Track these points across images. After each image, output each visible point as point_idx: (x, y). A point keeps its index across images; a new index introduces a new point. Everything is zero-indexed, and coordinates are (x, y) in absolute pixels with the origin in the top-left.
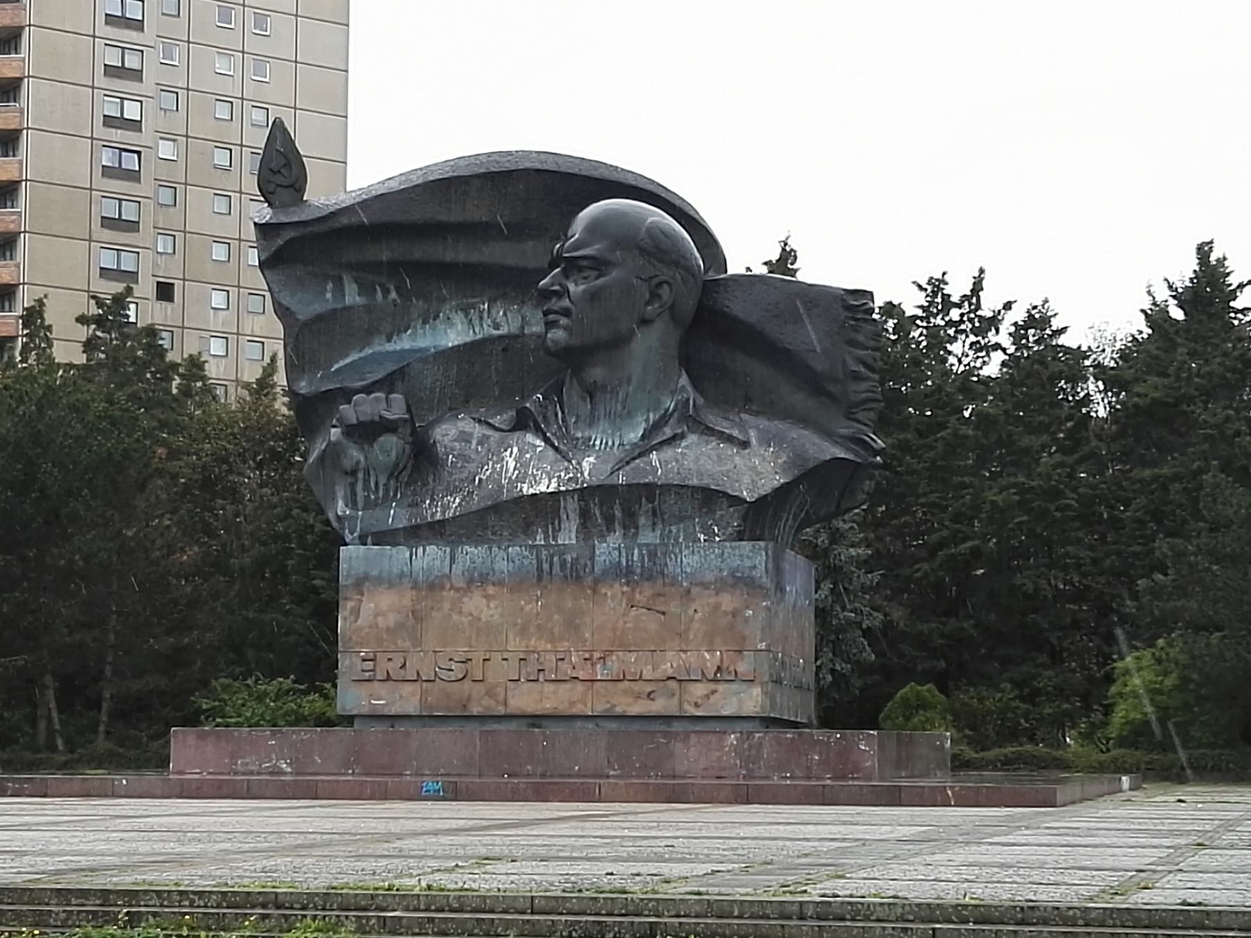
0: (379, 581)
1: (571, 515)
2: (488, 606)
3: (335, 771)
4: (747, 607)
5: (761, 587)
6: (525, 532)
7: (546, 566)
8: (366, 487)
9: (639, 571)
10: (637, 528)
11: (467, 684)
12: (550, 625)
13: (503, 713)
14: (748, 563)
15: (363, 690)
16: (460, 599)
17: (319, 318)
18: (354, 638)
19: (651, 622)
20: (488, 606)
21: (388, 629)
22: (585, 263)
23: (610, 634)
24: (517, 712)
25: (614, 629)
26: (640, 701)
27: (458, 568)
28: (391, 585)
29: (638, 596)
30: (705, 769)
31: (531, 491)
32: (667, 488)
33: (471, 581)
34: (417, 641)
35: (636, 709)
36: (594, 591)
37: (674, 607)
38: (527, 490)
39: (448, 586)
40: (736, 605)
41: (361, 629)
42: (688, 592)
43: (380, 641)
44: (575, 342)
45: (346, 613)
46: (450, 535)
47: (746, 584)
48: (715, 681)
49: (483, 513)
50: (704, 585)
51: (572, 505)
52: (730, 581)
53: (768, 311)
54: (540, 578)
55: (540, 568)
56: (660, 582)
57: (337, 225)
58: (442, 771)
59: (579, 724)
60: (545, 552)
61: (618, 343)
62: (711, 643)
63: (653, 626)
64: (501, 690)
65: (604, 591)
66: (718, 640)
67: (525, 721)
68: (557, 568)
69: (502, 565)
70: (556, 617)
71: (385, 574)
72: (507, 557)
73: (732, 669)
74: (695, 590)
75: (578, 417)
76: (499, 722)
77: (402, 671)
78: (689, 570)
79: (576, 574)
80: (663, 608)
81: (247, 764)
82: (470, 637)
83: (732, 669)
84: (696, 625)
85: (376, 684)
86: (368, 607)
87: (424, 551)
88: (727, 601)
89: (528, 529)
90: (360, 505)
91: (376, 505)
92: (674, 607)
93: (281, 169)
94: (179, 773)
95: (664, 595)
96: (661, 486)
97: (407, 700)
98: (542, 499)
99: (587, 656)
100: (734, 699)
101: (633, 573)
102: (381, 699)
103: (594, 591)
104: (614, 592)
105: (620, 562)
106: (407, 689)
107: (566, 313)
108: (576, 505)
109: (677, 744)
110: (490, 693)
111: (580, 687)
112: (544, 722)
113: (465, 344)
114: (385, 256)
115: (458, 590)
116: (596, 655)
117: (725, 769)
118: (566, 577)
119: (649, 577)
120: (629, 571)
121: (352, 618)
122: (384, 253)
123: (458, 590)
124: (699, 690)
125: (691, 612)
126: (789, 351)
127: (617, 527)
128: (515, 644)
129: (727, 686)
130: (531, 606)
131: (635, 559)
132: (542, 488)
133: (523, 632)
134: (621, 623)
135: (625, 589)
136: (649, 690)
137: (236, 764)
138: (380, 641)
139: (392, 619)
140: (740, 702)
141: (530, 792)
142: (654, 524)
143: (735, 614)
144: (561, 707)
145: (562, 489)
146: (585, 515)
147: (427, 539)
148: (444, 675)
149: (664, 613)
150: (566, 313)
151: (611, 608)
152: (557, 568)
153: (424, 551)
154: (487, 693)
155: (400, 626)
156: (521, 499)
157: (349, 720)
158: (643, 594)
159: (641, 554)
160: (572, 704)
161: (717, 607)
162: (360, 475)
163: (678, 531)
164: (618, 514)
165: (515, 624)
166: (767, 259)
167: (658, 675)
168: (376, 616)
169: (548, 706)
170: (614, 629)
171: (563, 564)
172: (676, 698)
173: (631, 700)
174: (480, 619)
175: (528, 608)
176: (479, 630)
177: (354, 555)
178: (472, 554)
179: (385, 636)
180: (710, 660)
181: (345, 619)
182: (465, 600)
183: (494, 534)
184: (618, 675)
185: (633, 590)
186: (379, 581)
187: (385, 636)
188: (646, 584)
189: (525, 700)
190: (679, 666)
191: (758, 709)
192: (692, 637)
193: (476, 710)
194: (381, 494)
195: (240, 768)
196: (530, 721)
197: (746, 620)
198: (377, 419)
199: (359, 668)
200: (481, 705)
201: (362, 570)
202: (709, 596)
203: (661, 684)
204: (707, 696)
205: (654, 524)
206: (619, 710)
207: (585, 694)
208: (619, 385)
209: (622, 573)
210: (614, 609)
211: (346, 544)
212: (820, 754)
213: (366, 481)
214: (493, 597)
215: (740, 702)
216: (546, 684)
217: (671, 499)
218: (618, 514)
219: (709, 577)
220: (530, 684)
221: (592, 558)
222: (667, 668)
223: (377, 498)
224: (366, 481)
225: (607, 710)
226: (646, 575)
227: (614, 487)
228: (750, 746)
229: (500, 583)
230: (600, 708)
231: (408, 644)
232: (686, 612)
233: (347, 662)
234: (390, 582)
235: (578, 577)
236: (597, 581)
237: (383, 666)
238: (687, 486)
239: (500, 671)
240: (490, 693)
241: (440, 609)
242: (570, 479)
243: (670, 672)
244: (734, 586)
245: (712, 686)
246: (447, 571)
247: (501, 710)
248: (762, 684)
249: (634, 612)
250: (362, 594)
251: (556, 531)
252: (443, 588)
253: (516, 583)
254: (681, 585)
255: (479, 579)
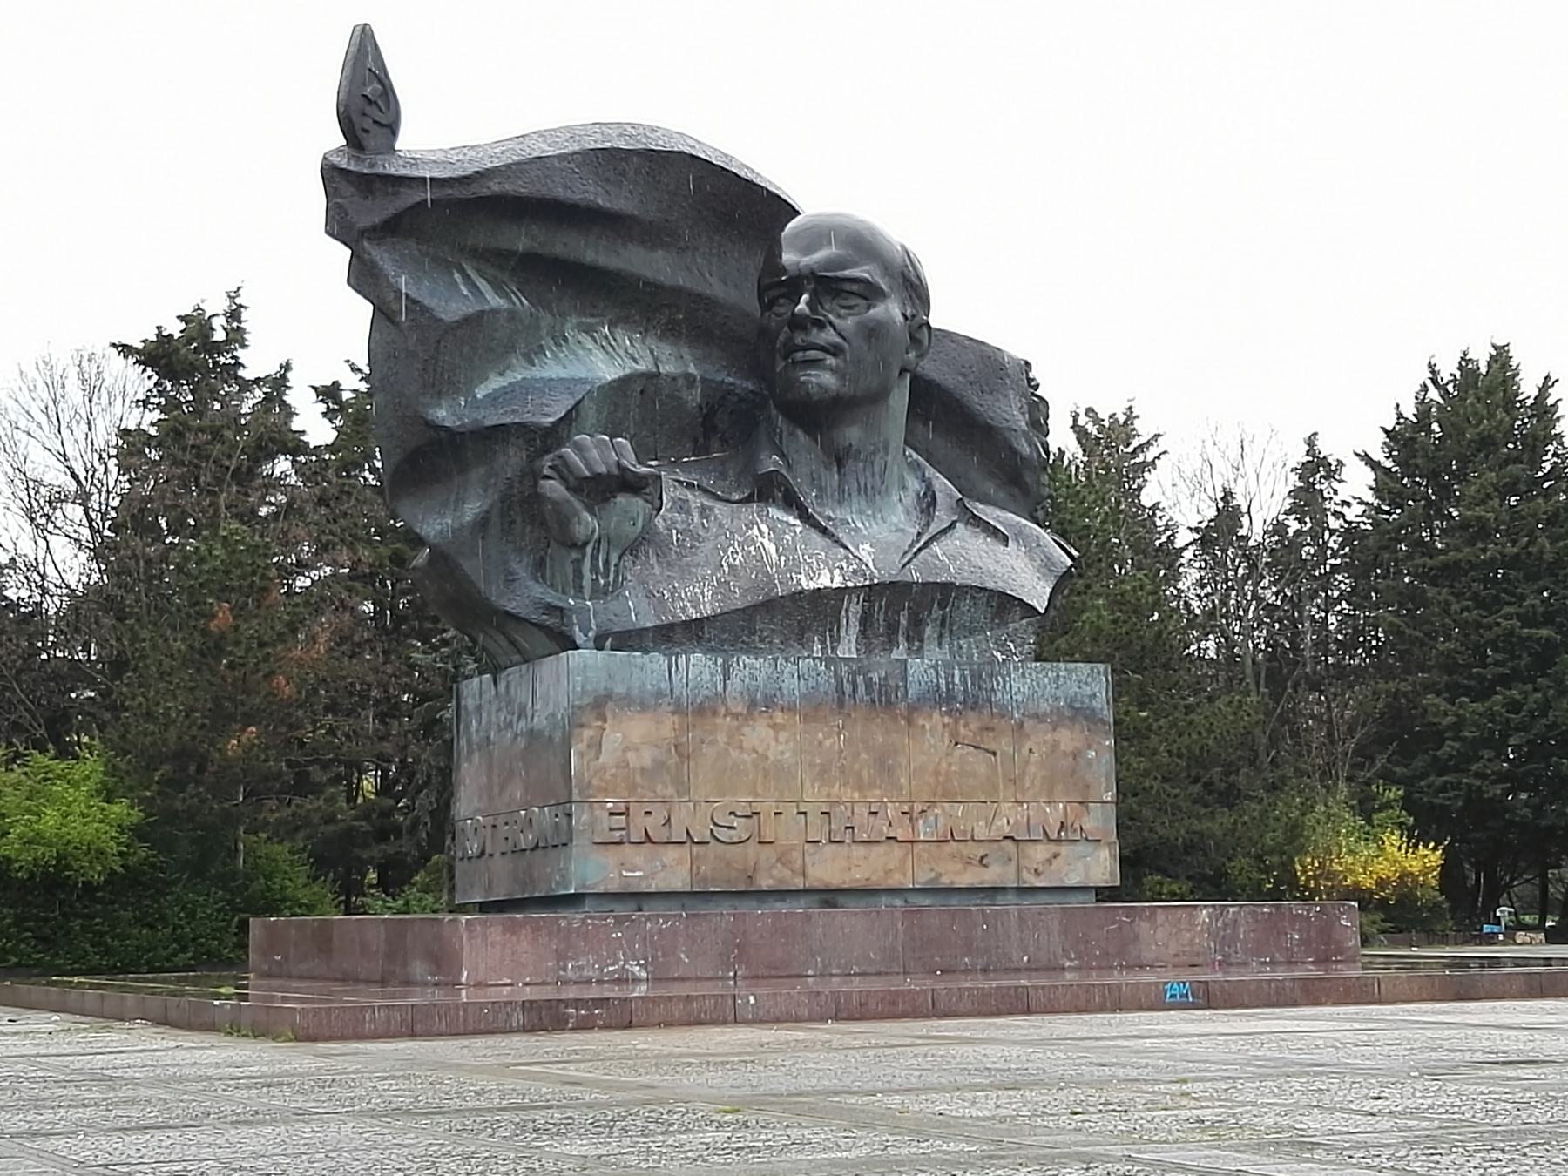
0: (627, 701)
1: (852, 620)
2: (777, 740)
3: (710, 974)
4: (1089, 747)
5: (1102, 720)
6: (800, 641)
7: (848, 687)
8: (594, 569)
9: (961, 698)
10: (921, 641)
11: (752, 847)
12: (857, 767)
13: (801, 887)
14: (1087, 690)
15: (610, 857)
16: (738, 728)
17: (467, 320)
18: (594, 782)
19: (978, 764)
20: (777, 740)
21: (643, 770)
22: (855, 288)
23: (932, 780)
24: (817, 885)
25: (937, 773)
26: (970, 868)
27: (735, 684)
28: (644, 707)
29: (962, 730)
30: (1176, 955)
31: (812, 585)
32: (965, 590)
33: (753, 704)
34: (683, 787)
35: (967, 879)
36: (909, 722)
37: (1004, 745)
38: (808, 584)
39: (723, 710)
40: (1078, 745)
41: (604, 768)
42: (1021, 725)
43: (632, 788)
44: (847, 390)
45: (582, 746)
46: (709, 640)
47: (1086, 718)
48: (1058, 841)
49: (749, 612)
50: (1038, 717)
51: (854, 608)
52: (1067, 713)
53: (964, 375)
54: (841, 704)
55: (840, 689)
56: (986, 711)
57: (485, 192)
58: (856, 969)
59: (884, 899)
60: (845, 669)
61: (878, 397)
62: (1050, 792)
63: (982, 769)
64: (796, 855)
65: (921, 722)
66: (1059, 788)
67: (816, 897)
68: (862, 689)
69: (790, 684)
70: (864, 756)
71: (635, 692)
72: (798, 672)
73: (1077, 826)
74: (1028, 724)
75: (820, 489)
76: (784, 900)
77: (665, 829)
78: (1020, 698)
79: (885, 699)
80: (992, 747)
81: (581, 968)
82: (755, 782)
83: (1077, 826)
84: (1032, 769)
85: (627, 848)
86: (613, 738)
87: (688, 661)
88: (1067, 739)
89: (802, 638)
90: (587, 592)
91: (606, 594)
92: (1004, 745)
93: (368, 104)
94: (479, 985)
95: (992, 729)
96: (961, 586)
97: (671, 871)
98: (825, 596)
99: (906, 809)
100: (1080, 865)
101: (955, 698)
102: (639, 869)
103: (909, 722)
104: (934, 722)
105: (938, 685)
106: (672, 854)
107: (835, 351)
108: (859, 608)
109: (1143, 924)
110: (783, 859)
111: (897, 851)
112: (841, 899)
113: (620, 379)
114: (522, 244)
115: (736, 716)
116: (917, 807)
117: (1198, 955)
118: (873, 701)
119: (973, 703)
120: (950, 697)
121: (592, 753)
122: (522, 240)
123: (736, 716)
124: (1040, 852)
125: (1025, 751)
126: (991, 427)
127: (901, 638)
128: (813, 794)
129: (1071, 847)
130: (831, 739)
131: (957, 681)
132: (824, 581)
133: (823, 774)
134: (944, 765)
135: (946, 720)
136: (981, 853)
137: (565, 970)
138: (632, 788)
139: (647, 757)
140: (1087, 868)
141: (1298, 992)
142: (941, 636)
143: (1075, 755)
144: (874, 878)
145: (850, 584)
146: (866, 620)
147: (682, 644)
148: (722, 834)
149: (994, 754)
150: (835, 351)
151: (931, 744)
152: (862, 689)
153: (688, 661)
154: (779, 860)
155: (659, 765)
156: (799, 596)
157: (575, 900)
158: (969, 727)
159: (962, 675)
160: (888, 872)
161: (1055, 745)
162: (589, 549)
163: (969, 647)
164: (903, 621)
165: (812, 765)
166: (251, 321)
167: (994, 835)
168: (624, 751)
169: (858, 876)
170: (937, 773)
171: (869, 684)
172: (1014, 863)
173: (960, 866)
174: (767, 758)
175: (827, 743)
176: (766, 773)
177: (590, 662)
178: (751, 668)
179: (638, 779)
180: (1054, 815)
181: (581, 755)
182: (746, 730)
183: (762, 640)
184: (945, 834)
185: (956, 722)
186: (627, 701)
187: (638, 779)
188: (971, 714)
189: (828, 869)
190: (1017, 821)
191: (1107, 877)
192: (1027, 784)
193: (765, 883)
194: (612, 576)
195: (570, 974)
196: (824, 896)
197: (1089, 763)
198: (615, 471)
199: (606, 826)
200: (771, 877)
201: (603, 685)
202: (1046, 733)
203: (995, 845)
204: (1049, 861)
205: (941, 636)
206: (945, 881)
207: (903, 860)
208: (874, 453)
209: (940, 698)
210: (935, 747)
211: (577, 648)
212: (1300, 932)
213: (595, 558)
214: (783, 727)
215: (1087, 868)
216: (854, 847)
217: (965, 605)
218: (903, 621)
219: (1045, 707)
220: (834, 846)
221: (905, 679)
222: (1003, 826)
223: (607, 584)
224: (595, 558)
225: (932, 880)
226: (969, 701)
227: (908, 585)
228: (1225, 925)
229: (790, 709)
230: (923, 878)
231: (670, 791)
232: (1019, 751)
233: (585, 817)
234: (644, 703)
235: (889, 702)
236: (912, 709)
237: (639, 822)
238: (985, 589)
239: (787, 831)
240: (783, 859)
241: (713, 742)
242: (855, 572)
243: (1007, 831)
244: (1072, 719)
245: (1054, 848)
246: (720, 688)
247: (799, 883)
248: (1109, 844)
249: (959, 750)
250: (605, 721)
251: (836, 640)
252: (715, 713)
253: (812, 708)
254: (1012, 717)
255: (762, 703)
